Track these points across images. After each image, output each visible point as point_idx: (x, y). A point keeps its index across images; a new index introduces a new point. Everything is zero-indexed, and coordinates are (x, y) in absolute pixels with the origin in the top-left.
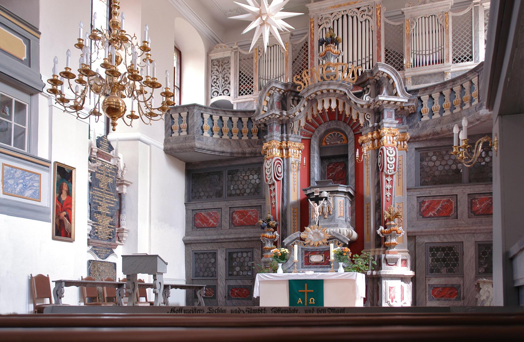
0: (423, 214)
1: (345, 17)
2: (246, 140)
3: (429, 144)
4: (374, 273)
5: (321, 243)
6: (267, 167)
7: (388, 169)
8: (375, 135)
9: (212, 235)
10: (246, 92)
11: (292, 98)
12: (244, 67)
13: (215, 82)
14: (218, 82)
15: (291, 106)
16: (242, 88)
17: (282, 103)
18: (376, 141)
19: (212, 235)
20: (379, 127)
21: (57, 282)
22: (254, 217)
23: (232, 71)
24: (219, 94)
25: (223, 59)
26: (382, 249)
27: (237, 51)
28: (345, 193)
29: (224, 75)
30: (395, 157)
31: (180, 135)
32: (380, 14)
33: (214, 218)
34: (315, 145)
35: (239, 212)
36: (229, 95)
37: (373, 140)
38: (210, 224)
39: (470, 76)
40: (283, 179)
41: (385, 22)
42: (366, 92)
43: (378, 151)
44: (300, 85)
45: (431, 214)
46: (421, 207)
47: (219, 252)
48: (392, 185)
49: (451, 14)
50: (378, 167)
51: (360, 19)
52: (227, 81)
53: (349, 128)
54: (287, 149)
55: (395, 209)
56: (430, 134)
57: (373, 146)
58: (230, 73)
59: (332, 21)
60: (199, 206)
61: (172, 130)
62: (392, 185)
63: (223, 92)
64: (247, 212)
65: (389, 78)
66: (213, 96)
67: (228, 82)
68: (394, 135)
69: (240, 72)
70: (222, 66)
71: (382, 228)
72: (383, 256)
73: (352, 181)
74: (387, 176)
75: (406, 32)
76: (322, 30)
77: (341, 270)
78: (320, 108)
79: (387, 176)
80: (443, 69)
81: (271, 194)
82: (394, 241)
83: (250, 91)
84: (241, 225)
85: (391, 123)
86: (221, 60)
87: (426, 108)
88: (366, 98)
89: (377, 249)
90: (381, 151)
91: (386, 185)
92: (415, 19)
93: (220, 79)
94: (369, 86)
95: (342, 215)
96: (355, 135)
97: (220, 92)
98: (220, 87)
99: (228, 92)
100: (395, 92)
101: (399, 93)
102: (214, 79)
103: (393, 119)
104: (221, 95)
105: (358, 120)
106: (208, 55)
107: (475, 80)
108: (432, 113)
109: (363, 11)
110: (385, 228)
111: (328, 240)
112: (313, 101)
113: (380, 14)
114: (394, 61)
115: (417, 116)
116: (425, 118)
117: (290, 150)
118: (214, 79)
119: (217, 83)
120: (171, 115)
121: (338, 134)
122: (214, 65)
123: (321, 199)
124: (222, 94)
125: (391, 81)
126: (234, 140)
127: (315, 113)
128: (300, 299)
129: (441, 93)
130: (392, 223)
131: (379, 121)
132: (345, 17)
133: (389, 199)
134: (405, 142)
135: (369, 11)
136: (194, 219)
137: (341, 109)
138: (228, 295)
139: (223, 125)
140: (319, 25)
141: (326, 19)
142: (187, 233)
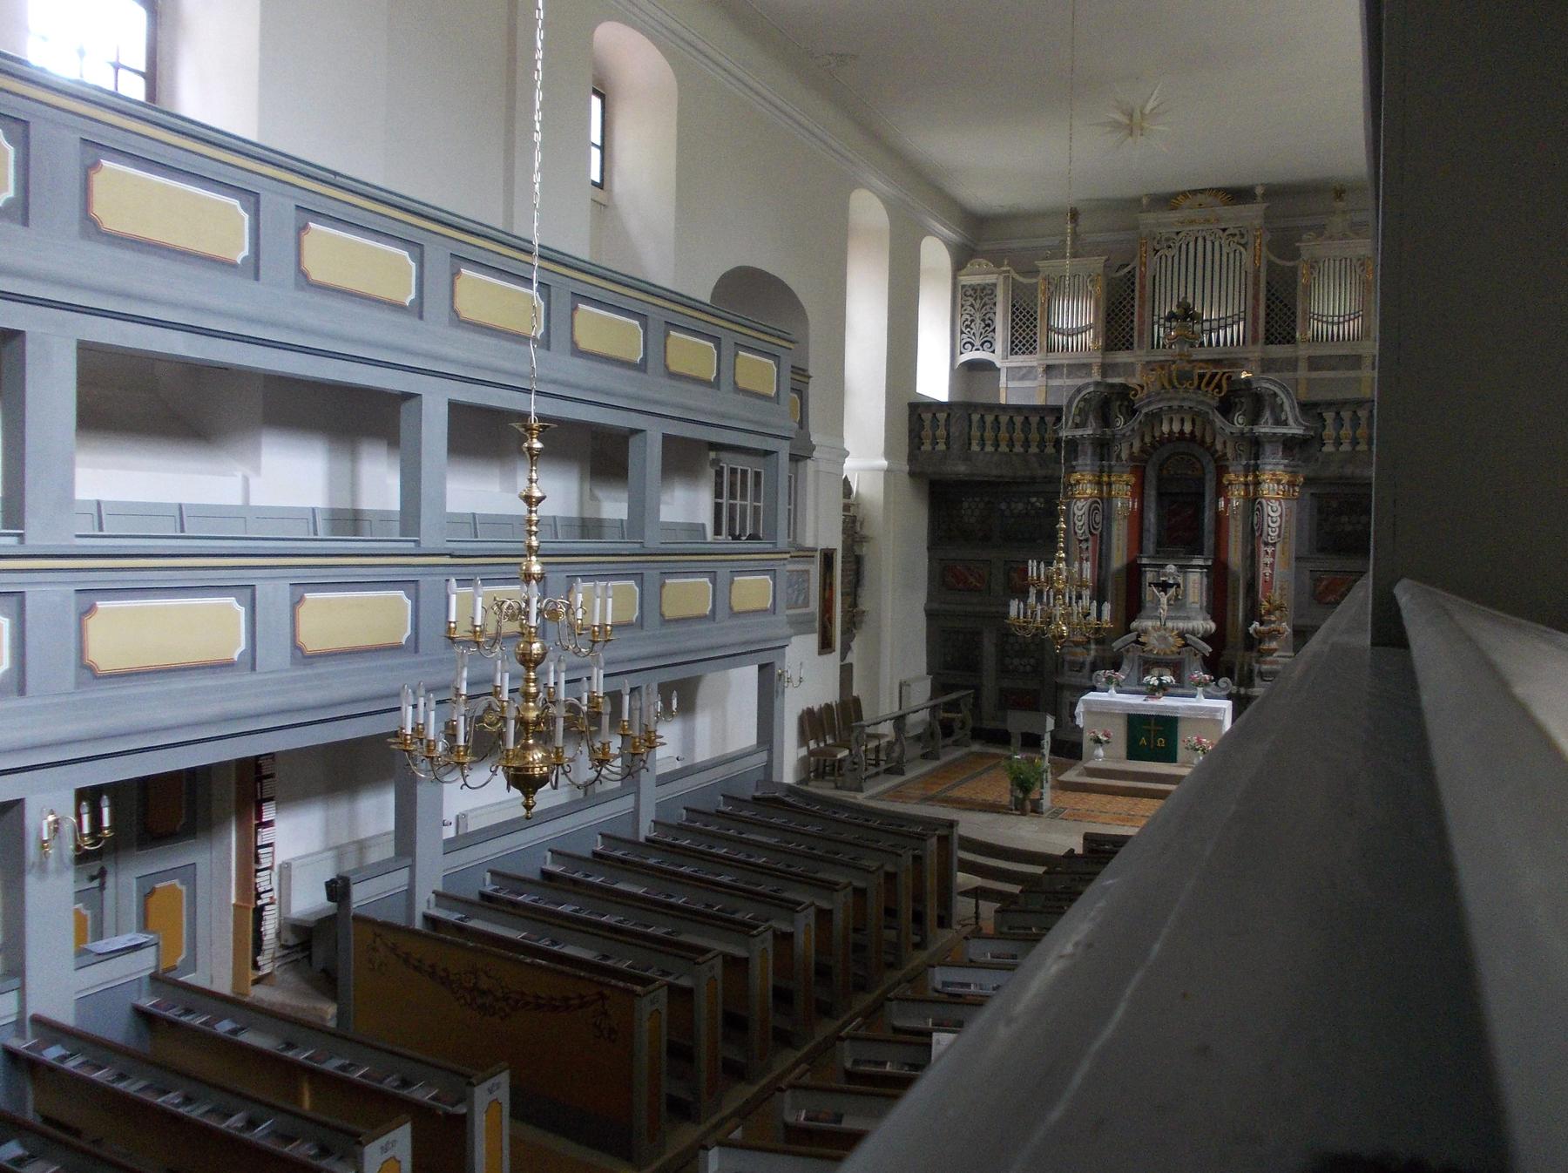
1: (1200, 241)
2: (1035, 455)
4: (1242, 691)
5: (1168, 652)
7: (1269, 535)
8: (1250, 478)
11: (1118, 403)
13: (967, 326)
14: (972, 326)
15: (1117, 417)
18: (1251, 488)
20: (1256, 467)
23: (999, 309)
24: (974, 348)
26: (1254, 654)
27: (1008, 277)
28: (1201, 567)
30: (1281, 516)
31: (934, 449)
34: (1151, 474)
36: (993, 352)
37: (1246, 484)
40: (1101, 533)
42: (1239, 406)
43: (1253, 503)
44: (1137, 391)
48: (1274, 558)
50: (1253, 530)
52: (989, 325)
54: (1109, 484)
55: (1276, 597)
57: (1247, 493)
58: (995, 313)
59: (1178, 245)
61: (920, 439)
62: (1274, 558)
63: (982, 345)
65: (1275, 395)
66: (963, 350)
67: (992, 328)
68: (1279, 482)
69: (1013, 306)
71: (1256, 624)
72: (1256, 667)
73: (1209, 542)
74: (1267, 544)
78: (1165, 428)
79: (1267, 544)
80: (1360, 351)
81: (1080, 553)
82: (1274, 645)
86: (979, 288)
87: (1329, 432)
88: (1239, 420)
89: (1246, 653)
90: (1259, 506)
91: (1264, 569)
93: (978, 321)
95: (1196, 600)
96: (1217, 467)
97: (977, 343)
98: (978, 334)
100: (1283, 418)
101: (1291, 421)
102: (967, 320)
104: (978, 350)
105: (1213, 443)
106: (955, 278)
108: (1338, 442)
109: (1231, 234)
110: (1261, 624)
112: (1155, 418)
114: (1277, 315)
116: (1329, 448)
117: (1114, 486)
118: (967, 320)
119: (972, 329)
120: (920, 415)
122: (967, 296)
123: (1171, 586)
124: (981, 348)
126: (1017, 454)
127: (1157, 434)
130: (1273, 618)
131: (1257, 457)
132: (1200, 241)
137: (1198, 433)
140: (1154, 250)
141: (1167, 240)
142: (931, 597)
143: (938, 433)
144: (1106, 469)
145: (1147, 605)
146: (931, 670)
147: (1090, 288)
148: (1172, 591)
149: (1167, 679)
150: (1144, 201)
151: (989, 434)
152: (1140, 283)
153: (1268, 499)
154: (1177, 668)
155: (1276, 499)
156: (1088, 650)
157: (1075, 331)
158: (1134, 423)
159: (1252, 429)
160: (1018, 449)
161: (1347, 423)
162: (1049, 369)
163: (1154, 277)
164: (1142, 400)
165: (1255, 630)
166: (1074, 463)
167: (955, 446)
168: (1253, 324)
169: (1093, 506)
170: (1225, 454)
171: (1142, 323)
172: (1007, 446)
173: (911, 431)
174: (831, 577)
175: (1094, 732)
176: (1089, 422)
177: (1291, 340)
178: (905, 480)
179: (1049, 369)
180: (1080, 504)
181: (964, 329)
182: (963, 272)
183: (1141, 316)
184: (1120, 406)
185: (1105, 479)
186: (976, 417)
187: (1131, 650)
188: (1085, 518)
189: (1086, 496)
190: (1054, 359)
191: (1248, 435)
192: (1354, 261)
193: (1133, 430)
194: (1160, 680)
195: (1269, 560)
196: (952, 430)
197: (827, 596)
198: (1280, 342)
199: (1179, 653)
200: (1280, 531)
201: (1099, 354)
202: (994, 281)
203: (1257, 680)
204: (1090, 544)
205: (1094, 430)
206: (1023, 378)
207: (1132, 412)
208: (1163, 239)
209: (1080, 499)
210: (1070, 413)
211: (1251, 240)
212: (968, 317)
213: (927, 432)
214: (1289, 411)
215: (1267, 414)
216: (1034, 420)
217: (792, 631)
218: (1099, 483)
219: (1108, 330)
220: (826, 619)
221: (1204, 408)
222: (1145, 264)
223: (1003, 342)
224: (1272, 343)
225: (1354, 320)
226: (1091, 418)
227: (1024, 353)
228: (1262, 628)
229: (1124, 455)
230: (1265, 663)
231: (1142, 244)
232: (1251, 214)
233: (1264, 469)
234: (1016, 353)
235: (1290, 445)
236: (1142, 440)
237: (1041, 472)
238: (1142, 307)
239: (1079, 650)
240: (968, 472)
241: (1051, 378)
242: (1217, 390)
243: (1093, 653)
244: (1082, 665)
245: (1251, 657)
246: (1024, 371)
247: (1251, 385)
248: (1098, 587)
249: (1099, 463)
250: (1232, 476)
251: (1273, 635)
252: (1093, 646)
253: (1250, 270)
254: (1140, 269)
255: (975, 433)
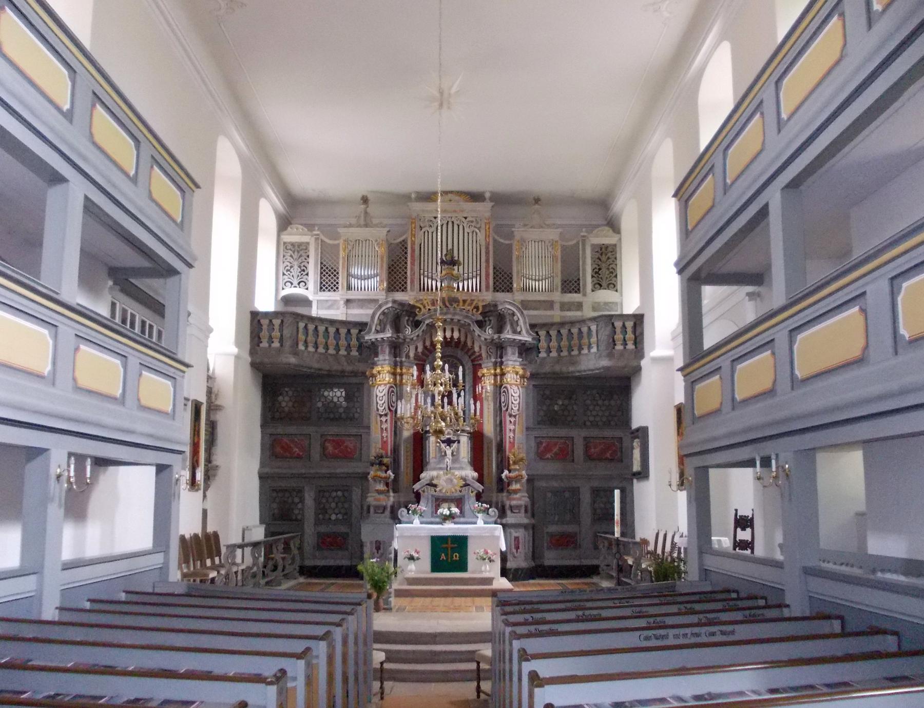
0: (541, 455)
2: (345, 356)
3: (546, 382)
6: (380, 395)
7: (512, 409)
8: (498, 371)
9: (298, 468)
10: (329, 288)
11: (407, 318)
12: (327, 258)
13: (288, 270)
14: (292, 270)
16: (324, 283)
17: (395, 322)
18: (499, 377)
19: (298, 468)
20: (502, 363)
21: (228, 547)
22: (352, 447)
23: (312, 260)
25: (300, 244)
26: (505, 494)
29: (301, 263)
32: (489, 228)
33: (299, 446)
35: (333, 441)
36: (307, 289)
37: (495, 375)
38: (294, 453)
39: (590, 324)
41: (494, 238)
42: (488, 323)
43: (499, 388)
44: (420, 309)
45: (548, 456)
46: (538, 447)
47: (306, 488)
48: (515, 425)
49: (560, 242)
51: (466, 230)
53: (467, 358)
54: (401, 375)
56: (549, 373)
57: (495, 380)
58: (308, 263)
59: (435, 225)
60: (280, 430)
61: (259, 338)
63: (299, 284)
64: (344, 442)
66: (284, 287)
68: (517, 373)
69: (321, 263)
70: (298, 252)
72: (507, 503)
74: (511, 416)
75: (515, 253)
76: (425, 232)
77: (480, 523)
79: (511, 416)
80: (553, 299)
83: (335, 288)
84: (335, 457)
85: (515, 361)
87: (543, 344)
88: (489, 331)
89: (499, 494)
92: (525, 242)
93: (296, 267)
94: (491, 318)
96: (473, 365)
97: (295, 282)
98: (295, 276)
99: (306, 284)
100: (519, 329)
101: (524, 332)
102: (287, 266)
103: (515, 357)
104: (295, 287)
105: (473, 347)
107: (594, 328)
108: (549, 351)
111: (461, 487)
113: (489, 228)
115: (535, 353)
116: (543, 354)
118: (287, 266)
120: (259, 321)
121: (453, 361)
123: (454, 442)
125: (515, 318)
126: (331, 355)
128: (443, 554)
129: (559, 332)
131: (501, 357)
133: (512, 440)
134: (525, 380)
135: (478, 223)
136: (272, 446)
137: (462, 339)
138: (318, 544)
139: (318, 336)
140: (420, 227)
142: (263, 465)
143: (273, 334)
144: (399, 364)
145: (431, 461)
146: (262, 521)
147: (377, 249)
148: (455, 445)
149: (455, 510)
150: (413, 196)
151: (311, 338)
152: (412, 248)
153: (511, 385)
154: (459, 502)
155: (516, 385)
156: (388, 497)
157: (366, 277)
158: (419, 331)
159: (499, 337)
160: (332, 351)
161: (554, 338)
162: (348, 302)
163: (420, 245)
164: (424, 315)
165: (506, 477)
166: (376, 359)
167: (288, 344)
168: (486, 279)
169: (390, 390)
170: (480, 355)
171: (413, 274)
172: (324, 348)
173: (252, 333)
174: (199, 425)
175: (408, 551)
176: (387, 329)
177: (509, 289)
178: (248, 368)
179: (348, 302)
180: (381, 388)
181: (285, 272)
182: (285, 232)
183: (412, 269)
184: (408, 321)
185: (398, 370)
186: (302, 325)
187: (426, 490)
188: (385, 398)
189: (384, 382)
190: (352, 295)
191: (497, 340)
192: (547, 242)
193: (418, 336)
194: (450, 511)
195: (512, 427)
196: (285, 332)
197: (196, 441)
198: (503, 291)
199: (460, 491)
200: (519, 407)
201: (384, 293)
202: (307, 240)
203: (508, 512)
204: (388, 418)
205: (392, 334)
206: (329, 308)
207: (417, 324)
208: (426, 220)
209: (380, 385)
210: (373, 322)
211: (483, 226)
212: (288, 264)
213: (264, 334)
214: (523, 326)
215: (508, 327)
216: (343, 331)
217: (339, 230)
218: (394, 374)
219: (389, 278)
220: (195, 462)
221: (468, 321)
222: (415, 235)
223: (314, 283)
224: (498, 291)
225: (542, 280)
226: (388, 327)
227: (329, 290)
228: (511, 474)
229: (412, 355)
230: (514, 499)
231: (412, 223)
232: (483, 209)
233: (507, 364)
234: (324, 290)
235: (525, 350)
236: (424, 343)
237: (349, 368)
238: (413, 264)
239: (382, 497)
240: (297, 363)
241: (350, 308)
242: (475, 310)
243: (392, 499)
244: (385, 508)
245: (502, 496)
246: (330, 303)
247: (497, 308)
248: (394, 449)
249: (394, 359)
250: (485, 371)
251: (518, 479)
252: (392, 494)
253: (483, 243)
254: (411, 238)
255: (302, 337)
